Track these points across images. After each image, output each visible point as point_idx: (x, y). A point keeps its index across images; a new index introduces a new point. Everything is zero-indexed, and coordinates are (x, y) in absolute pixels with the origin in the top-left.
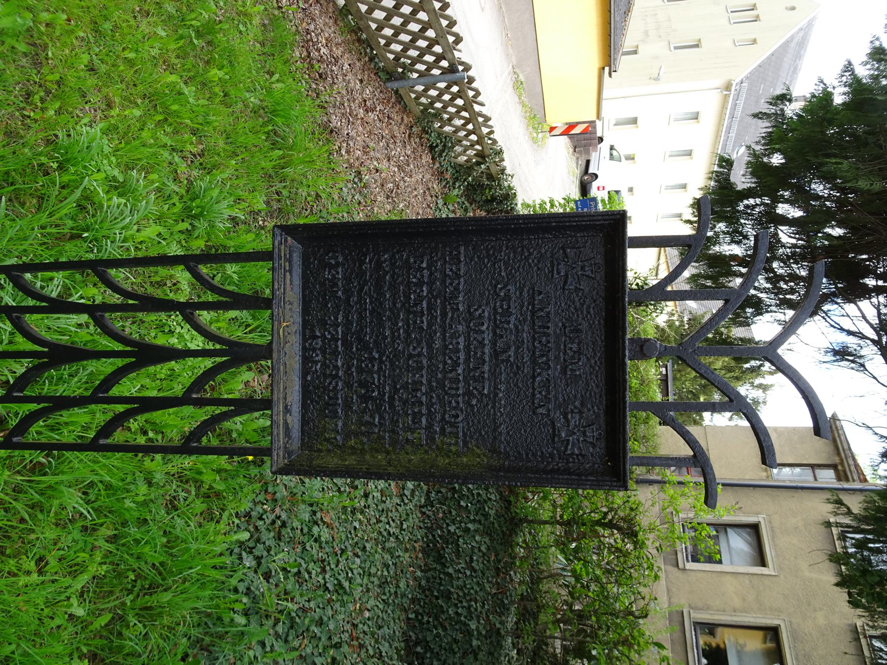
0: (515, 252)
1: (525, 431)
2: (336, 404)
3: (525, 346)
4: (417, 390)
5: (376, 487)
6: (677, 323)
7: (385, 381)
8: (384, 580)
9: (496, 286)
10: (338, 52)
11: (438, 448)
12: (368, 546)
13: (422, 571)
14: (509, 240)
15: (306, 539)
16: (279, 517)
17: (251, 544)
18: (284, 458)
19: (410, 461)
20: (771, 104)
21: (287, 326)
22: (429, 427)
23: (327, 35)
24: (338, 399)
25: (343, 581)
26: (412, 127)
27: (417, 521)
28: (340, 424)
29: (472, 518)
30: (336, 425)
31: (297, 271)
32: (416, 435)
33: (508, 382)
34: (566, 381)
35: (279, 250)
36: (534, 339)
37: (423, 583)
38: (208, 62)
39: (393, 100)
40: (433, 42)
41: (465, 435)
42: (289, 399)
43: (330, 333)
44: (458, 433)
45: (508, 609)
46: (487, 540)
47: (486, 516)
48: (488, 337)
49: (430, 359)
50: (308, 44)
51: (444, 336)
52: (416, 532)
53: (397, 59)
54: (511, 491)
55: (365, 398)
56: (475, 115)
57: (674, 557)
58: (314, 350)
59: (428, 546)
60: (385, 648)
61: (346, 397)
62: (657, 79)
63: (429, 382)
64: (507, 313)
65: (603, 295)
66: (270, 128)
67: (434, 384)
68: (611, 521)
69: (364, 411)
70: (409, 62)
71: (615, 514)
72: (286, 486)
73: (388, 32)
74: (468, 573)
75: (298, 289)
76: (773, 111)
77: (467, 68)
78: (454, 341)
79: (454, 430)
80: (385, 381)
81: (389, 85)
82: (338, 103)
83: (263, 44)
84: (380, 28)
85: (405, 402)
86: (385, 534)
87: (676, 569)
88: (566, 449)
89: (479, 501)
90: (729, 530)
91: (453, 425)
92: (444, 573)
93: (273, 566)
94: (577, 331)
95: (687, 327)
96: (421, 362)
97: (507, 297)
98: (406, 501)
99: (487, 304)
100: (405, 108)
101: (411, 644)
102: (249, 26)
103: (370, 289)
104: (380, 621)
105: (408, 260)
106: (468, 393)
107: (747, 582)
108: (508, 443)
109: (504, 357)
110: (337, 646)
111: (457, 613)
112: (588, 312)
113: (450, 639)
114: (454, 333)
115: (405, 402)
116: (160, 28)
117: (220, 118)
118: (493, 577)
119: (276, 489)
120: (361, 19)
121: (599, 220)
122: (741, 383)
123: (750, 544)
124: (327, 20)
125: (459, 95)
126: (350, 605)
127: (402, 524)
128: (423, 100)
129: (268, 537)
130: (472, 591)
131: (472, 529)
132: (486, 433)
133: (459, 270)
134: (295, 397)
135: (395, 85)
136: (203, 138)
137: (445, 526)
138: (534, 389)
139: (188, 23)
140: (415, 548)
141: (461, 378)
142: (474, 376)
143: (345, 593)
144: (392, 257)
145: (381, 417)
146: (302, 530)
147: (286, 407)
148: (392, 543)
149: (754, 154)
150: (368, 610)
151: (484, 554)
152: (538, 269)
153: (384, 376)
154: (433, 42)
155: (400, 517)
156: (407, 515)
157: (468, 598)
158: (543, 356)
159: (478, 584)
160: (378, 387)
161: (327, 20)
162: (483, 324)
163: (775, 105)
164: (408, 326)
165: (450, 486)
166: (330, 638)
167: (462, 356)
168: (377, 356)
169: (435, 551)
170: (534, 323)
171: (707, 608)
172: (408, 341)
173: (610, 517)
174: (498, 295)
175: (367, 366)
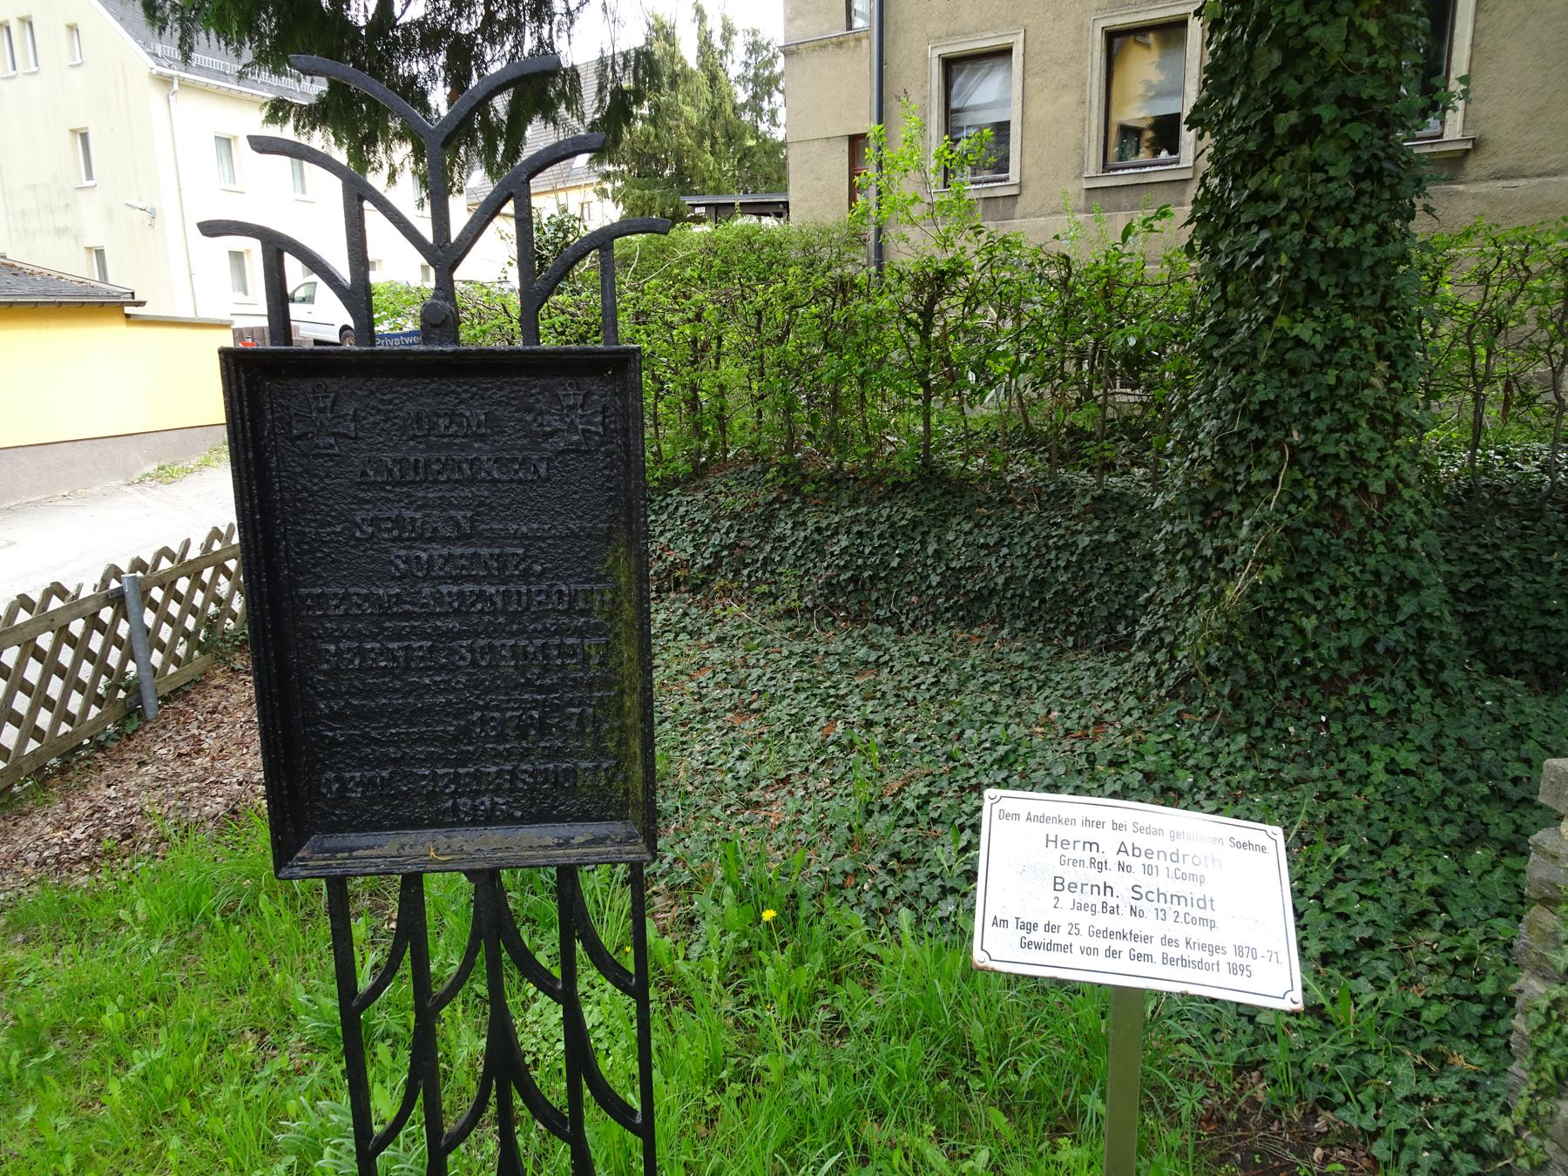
0: (304, 512)
1: (576, 493)
2: (556, 773)
3: (447, 495)
4: (526, 654)
5: (858, 709)
6: (619, 184)
7: (516, 701)
8: (1009, 690)
9: (358, 539)
10: (82, 807)
11: (610, 619)
12: (948, 717)
13: (1002, 628)
14: (285, 521)
15: (923, 820)
16: (884, 864)
17: (922, 905)
18: (635, 844)
19: (630, 659)
20: (163, 29)
21: (437, 850)
22: (580, 632)
23: (48, 829)
24: (546, 770)
25: (995, 755)
26: (233, 670)
27: (921, 638)
28: (584, 764)
29: (918, 547)
30: (586, 769)
31: (353, 839)
32: (593, 652)
33: (504, 518)
34: (496, 433)
35: (314, 868)
36: (436, 482)
37: (1020, 624)
38: (91, 1034)
39: (181, 706)
40: (63, 636)
41: (587, 581)
42: (549, 841)
43: (446, 786)
44: (585, 591)
45: (1064, 484)
46: (955, 521)
47: (915, 523)
48: (438, 550)
49: (477, 635)
50: (63, 863)
51: (440, 614)
52: (938, 640)
53: (99, 701)
54: (878, 482)
55: (543, 729)
56: (208, 557)
57: (1001, 202)
58: (475, 808)
59: (963, 618)
60: (1108, 684)
61: (543, 757)
62: (153, 214)
63: (512, 635)
64: (398, 522)
65: (362, 380)
66: (218, 918)
67: (515, 627)
68: (921, 315)
69: (563, 729)
70: (104, 678)
71: (910, 306)
72: (835, 856)
73: (44, 719)
74: (1005, 551)
75: (381, 838)
76: (176, 26)
77: (114, 572)
78: (447, 599)
79: (581, 595)
80: (516, 701)
81: (150, 714)
82: (180, 804)
83: (61, 943)
84: (38, 734)
85: (546, 670)
86: (934, 690)
87: (1020, 199)
88: (597, 433)
89: (892, 536)
90: (954, 105)
91: (573, 599)
92: (1005, 590)
93: (957, 870)
94: (418, 418)
95: (624, 167)
96: (482, 647)
97: (373, 522)
98: (887, 657)
99: (387, 552)
100: (198, 683)
101: (1113, 641)
102: (26, 968)
103: (375, 728)
104: (1069, 693)
105: (325, 673)
106: (526, 576)
107: (1036, 80)
108: (595, 517)
109: (466, 526)
110: (1092, 760)
111: (1066, 568)
112: (390, 402)
113: (1106, 578)
114: (435, 600)
115: (546, 670)
116: (19, 1118)
117: (196, 1006)
118: (1014, 510)
119: (838, 870)
120: (20, 769)
121: (239, 388)
122: (722, 74)
123: (991, 68)
124: (21, 830)
125: (168, 585)
126: (1035, 741)
127: (923, 663)
128: (181, 650)
129: (914, 878)
130: (1033, 544)
131: (935, 546)
132: (582, 549)
133: (335, 595)
134: (547, 834)
135: (150, 702)
136: (232, 1032)
137: (931, 592)
138: (512, 481)
139: (15, 1072)
140: (963, 641)
141: (502, 588)
142: (498, 569)
143: (1014, 751)
144: (322, 696)
145: (570, 703)
146: (908, 826)
147: (559, 845)
148: (951, 680)
149: (261, 59)
150: (1049, 712)
151: (977, 525)
152: (327, 476)
153: (508, 701)
154: (63, 636)
155: (910, 666)
156: (908, 655)
157: (1044, 550)
158: (460, 469)
159: (1022, 534)
160: (525, 710)
161: (21, 830)
162: (418, 558)
163: (164, 22)
164: (430, 668)
165: (868, 585)
166: (1080, 772)
167: (468, 587)
168: (478, 714)
169: (971, 607)
170: (412, 482)
171: (1080, 148)
172: (453, 669)
173: (915, 316)
174: (372, 536)
175: (494, 728)
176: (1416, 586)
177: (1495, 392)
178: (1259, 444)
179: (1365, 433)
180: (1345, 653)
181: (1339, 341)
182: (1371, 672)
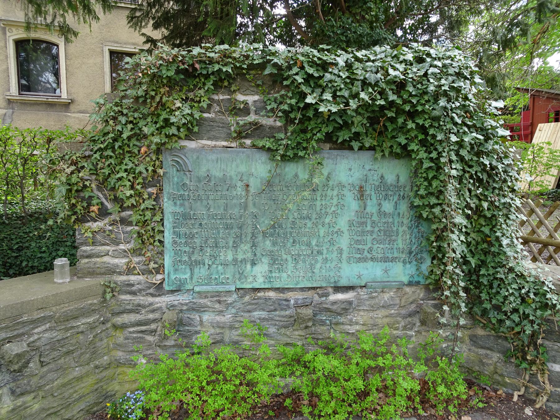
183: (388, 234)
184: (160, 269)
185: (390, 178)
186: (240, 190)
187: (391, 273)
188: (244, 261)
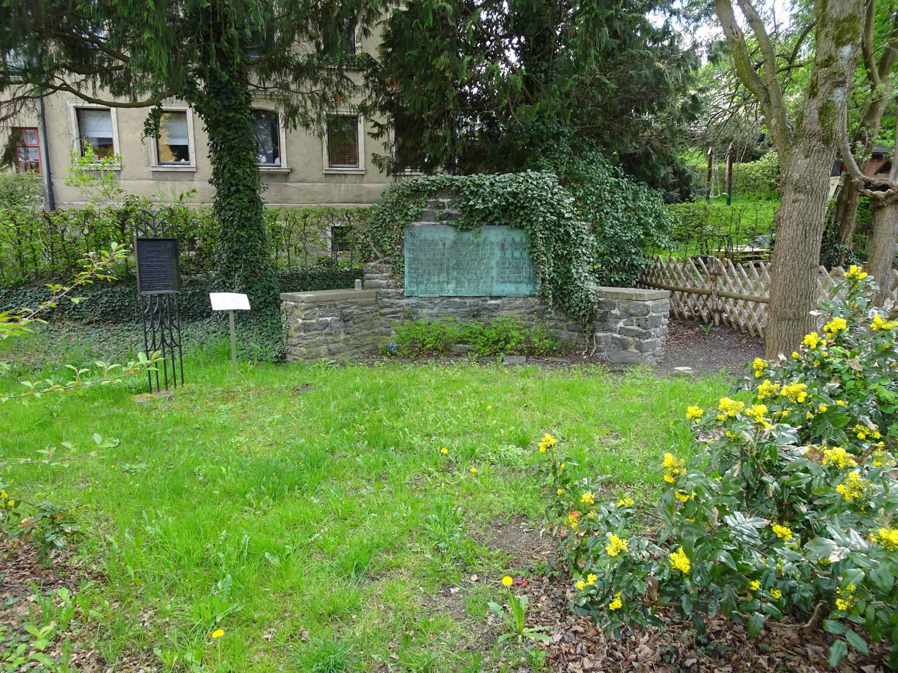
176: (273, 288)
177: (292, 249)
178: (236, 259)
179: (258, 256)
180: (260, 303)
181: (250, 236)
182: (266, 307)
183: (518, 269)
184: (402, 286)
185: (518, 239)
186: (441, 246)
187: (520, 289)
188: (443, 282)
